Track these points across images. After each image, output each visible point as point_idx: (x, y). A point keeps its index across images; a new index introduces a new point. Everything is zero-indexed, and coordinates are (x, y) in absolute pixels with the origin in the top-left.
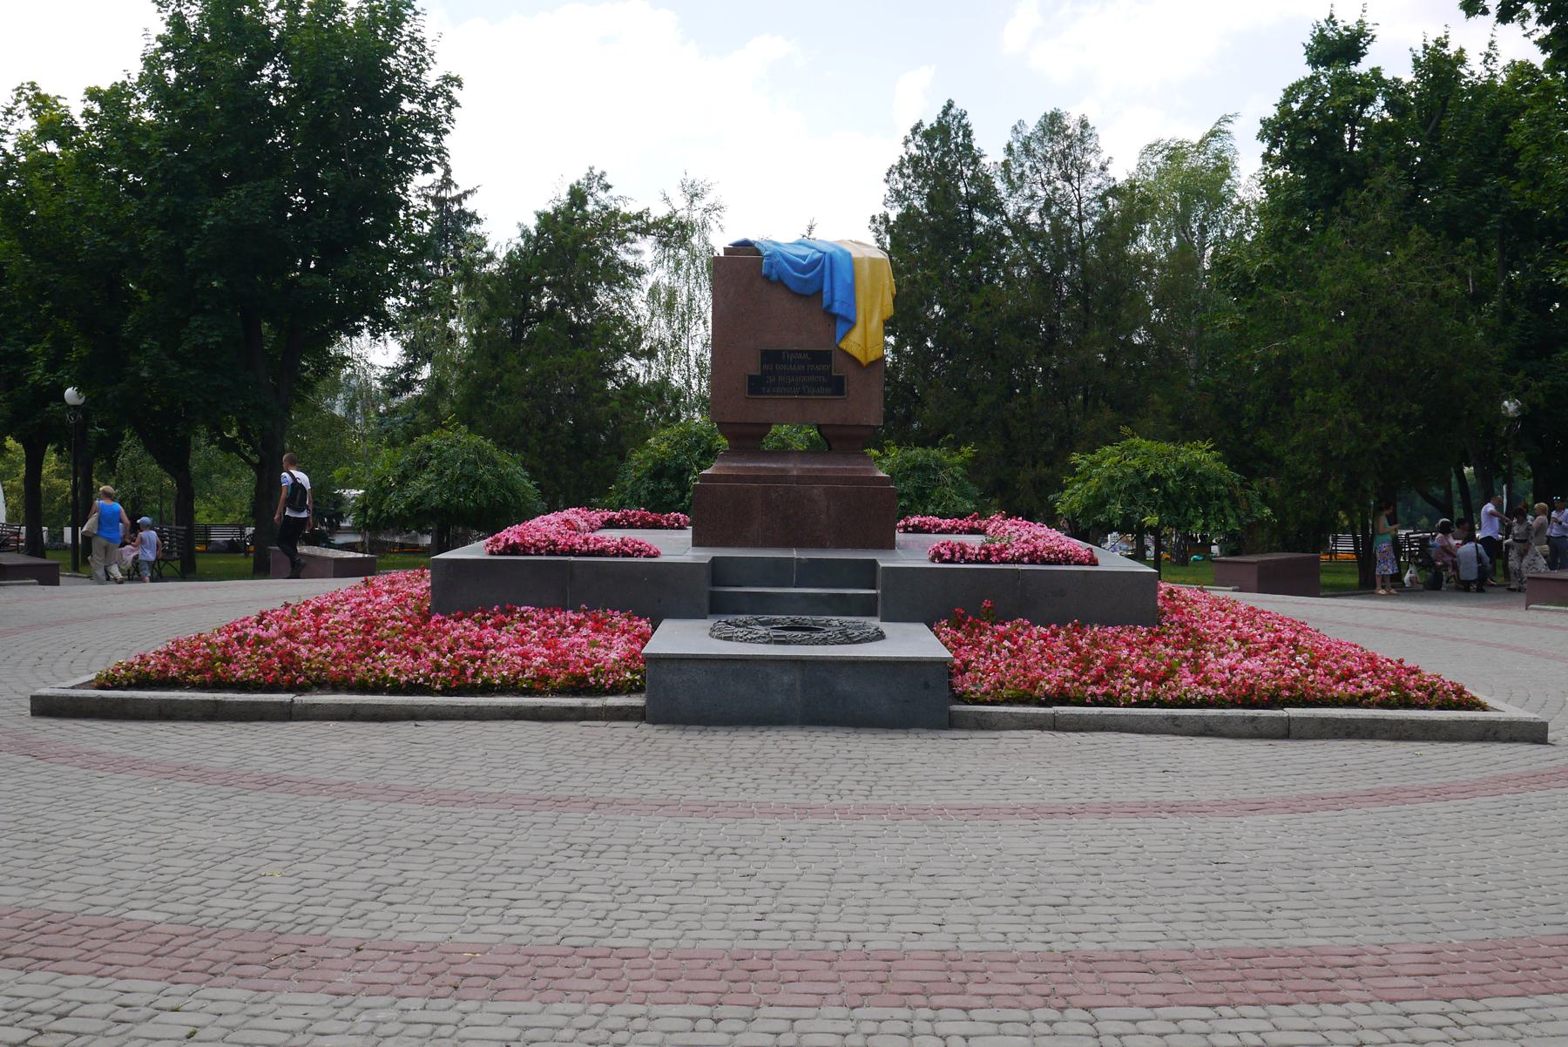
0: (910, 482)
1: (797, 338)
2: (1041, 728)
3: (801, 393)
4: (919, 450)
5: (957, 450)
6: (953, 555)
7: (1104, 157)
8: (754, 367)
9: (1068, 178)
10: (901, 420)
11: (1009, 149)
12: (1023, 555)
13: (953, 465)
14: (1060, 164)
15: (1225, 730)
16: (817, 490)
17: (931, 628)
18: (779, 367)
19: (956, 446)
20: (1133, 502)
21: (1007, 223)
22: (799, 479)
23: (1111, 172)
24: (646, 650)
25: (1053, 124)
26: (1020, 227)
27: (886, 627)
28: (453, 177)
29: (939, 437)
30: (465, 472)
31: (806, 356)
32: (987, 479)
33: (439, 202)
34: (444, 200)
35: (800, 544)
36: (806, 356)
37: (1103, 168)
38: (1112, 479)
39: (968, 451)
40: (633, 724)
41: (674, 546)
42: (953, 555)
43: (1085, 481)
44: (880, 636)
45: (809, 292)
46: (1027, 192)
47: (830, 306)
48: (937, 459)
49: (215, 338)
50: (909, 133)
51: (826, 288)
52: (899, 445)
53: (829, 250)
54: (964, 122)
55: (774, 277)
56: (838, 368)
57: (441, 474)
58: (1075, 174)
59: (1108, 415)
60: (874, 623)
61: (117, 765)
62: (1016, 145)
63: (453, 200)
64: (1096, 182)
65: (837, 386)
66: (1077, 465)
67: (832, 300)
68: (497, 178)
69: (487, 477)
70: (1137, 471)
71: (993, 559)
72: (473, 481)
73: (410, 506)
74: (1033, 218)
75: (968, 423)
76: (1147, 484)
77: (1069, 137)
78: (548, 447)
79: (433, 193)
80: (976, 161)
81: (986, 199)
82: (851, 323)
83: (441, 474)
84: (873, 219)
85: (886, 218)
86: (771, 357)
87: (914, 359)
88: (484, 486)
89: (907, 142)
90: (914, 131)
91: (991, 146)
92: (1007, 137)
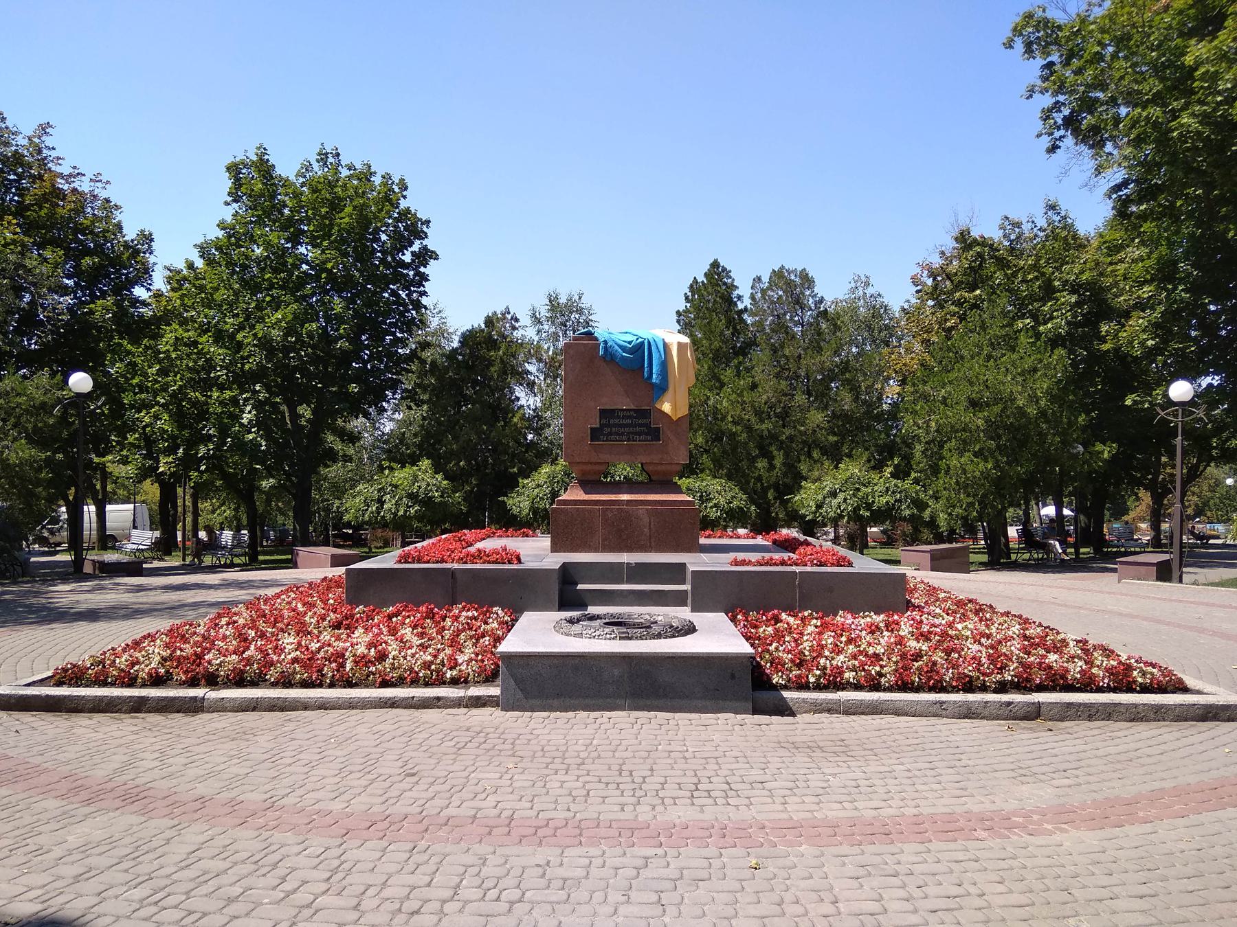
2: (829, 711)
15: (986, 712)
17: (734, 620)
22: (153, 559)
24: (504, 647)
27: (698, 618)
35: (630, 549)
40: (624, 713)
41: (536, 551)
44: (690, 629)
60: (683, 613)
61: (85, 793)
68: (455, 303)
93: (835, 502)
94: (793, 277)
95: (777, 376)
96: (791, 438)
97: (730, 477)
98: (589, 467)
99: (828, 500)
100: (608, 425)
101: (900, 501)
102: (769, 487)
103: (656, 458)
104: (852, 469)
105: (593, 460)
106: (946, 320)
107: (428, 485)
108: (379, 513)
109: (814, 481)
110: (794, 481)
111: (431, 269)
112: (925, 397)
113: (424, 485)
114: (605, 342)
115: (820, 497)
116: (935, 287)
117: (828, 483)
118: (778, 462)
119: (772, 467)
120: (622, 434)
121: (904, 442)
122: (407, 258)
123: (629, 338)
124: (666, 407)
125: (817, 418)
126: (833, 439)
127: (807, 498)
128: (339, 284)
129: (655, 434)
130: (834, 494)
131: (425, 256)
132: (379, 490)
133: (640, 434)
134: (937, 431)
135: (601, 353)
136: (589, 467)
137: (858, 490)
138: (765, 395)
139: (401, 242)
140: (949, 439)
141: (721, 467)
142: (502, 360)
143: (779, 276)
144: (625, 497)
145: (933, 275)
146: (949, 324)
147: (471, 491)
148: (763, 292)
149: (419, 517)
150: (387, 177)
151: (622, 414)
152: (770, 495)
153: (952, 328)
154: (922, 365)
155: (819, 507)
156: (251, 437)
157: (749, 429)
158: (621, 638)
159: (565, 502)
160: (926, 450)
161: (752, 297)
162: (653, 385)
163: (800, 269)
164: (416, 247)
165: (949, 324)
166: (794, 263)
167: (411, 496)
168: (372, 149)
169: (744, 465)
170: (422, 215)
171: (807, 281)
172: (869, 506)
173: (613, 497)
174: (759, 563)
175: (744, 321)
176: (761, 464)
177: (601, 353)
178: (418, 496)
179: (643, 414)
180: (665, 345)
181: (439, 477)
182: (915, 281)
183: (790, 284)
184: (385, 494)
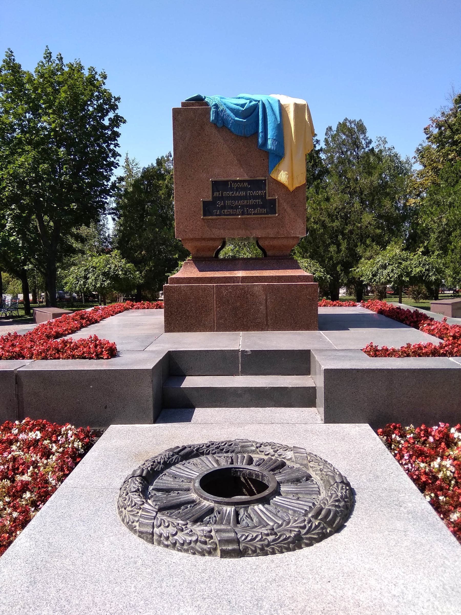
8: (207, 195)
18: (225, 194)
36: (246, 184)
93: (385, 272)
94: (353, 126)
95: (343, 192)
96: (351, 232)
97: (312, 257)
98: (204, 244)
99: (380, 271)
100: (222, 198)
101: (428, 270)
102: (338, 263)
103: (271, 233)
104: (395, 249)
105: (206, 236)
106: (448, 154)
107: (116, 266)
108: (85, 285)
109: (369, 259)
110: (355, 259)
111: (121, 129)
112: (438, 203)
113: (113, 266)
114: (216, 106)
115: (375, 269)
116: (441, 134)
117: (380, 259)
118: (343, 247)
119: (339, 251)
120: (236, 207)
121: (422, 232)
122: (106, 122)
123: (242, 101)
124: (282, 176)
125: (368, 218)
126: (378, 231)
127: (364, 269)
128: (61, 139)
129: (270, 206)
130: (384, 267)
131: (117, 121)
132: (85, 270)
133: (254, 206)
134: (446, 224)
135: (212, 118)
136: (204, 244)
137: (401, 263)
138: (336, 203)
139: (103, 113)
140: (455, 230)
141: (306, 252)
142: (167, 186)
143: (342, 127)
144: (240, 274)
145: (439, 126)
146: (450, 157)
147: (150, 270)
148: (333, 137)
149: (111, 287)
150: (91, 69)
151: (235, 186)
152: (338, 269)
153: (452, 159)
154: (433, 183)
155: (374, 275)
156: (12, 238)
157: (324, 225)
158: (225, 554)
159: (178, 280)
160: (439, 237)
161: (326, 141)
162: (268, 153)
163: (357, 120)
164: (111, 115)
165: (450, 157)
166: (354, 117)
167: (104, 274)
168: (81, 52)
169: (321, 250)
170: (115, 94)
171: (362, 128)
172: (408, 274)
173: (227, 274)
174: (406, 353)
175: (319, 157)
176: (333, 248)
177: (212, 118)
178: (109, 274)
179: (258, 184)
180: (282, 108)
181: (124, 261)
182: (426, 130)
183: (351, 131)
184: (89, 273)
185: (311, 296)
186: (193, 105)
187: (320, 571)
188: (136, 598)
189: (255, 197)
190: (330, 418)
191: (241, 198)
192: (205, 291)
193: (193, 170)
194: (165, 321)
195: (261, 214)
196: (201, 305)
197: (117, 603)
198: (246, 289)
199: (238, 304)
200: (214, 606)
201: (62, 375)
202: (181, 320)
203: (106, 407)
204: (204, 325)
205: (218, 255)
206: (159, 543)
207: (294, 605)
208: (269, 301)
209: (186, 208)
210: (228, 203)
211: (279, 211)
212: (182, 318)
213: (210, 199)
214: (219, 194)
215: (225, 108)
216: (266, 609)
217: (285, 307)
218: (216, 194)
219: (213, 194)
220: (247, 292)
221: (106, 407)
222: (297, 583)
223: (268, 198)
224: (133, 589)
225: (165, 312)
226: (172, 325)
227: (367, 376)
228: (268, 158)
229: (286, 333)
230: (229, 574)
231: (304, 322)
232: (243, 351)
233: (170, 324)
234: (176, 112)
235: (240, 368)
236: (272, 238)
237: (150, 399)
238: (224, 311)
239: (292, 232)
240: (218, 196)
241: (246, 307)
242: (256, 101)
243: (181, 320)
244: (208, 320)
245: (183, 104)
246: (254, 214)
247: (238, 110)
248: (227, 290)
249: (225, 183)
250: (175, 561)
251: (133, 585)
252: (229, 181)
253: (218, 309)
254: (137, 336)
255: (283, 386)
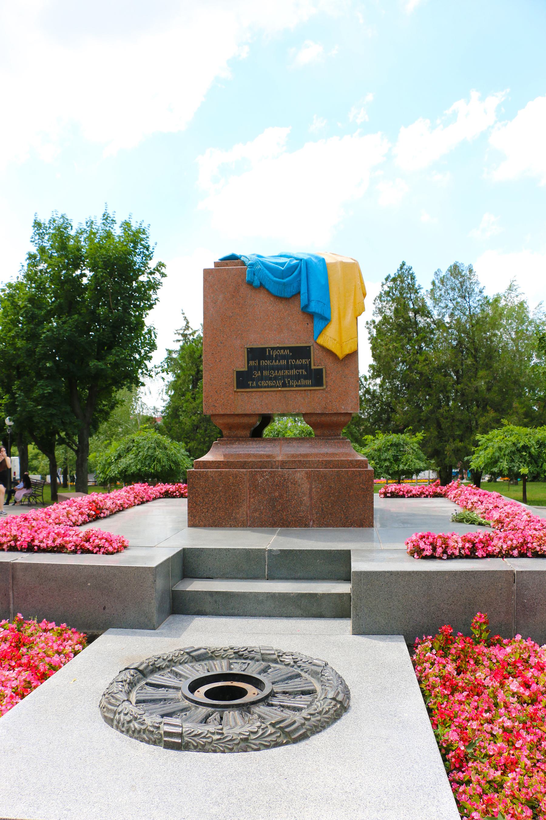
0: (390, 452)
1: (276, 330)
3: (284, 385)
4: (394, 435)
5: (414, 434)
6: (434, 549)
7: (481, 286)
9: (464, 297)
10: (384, 417)
11: (433, 283)
12: (512, 548)
13: (413, 443)
14: (459, 290)
16: (300, 474)
18: (264, 363)
19: (413, 433)
20: (512, 461)
21: (434, 322)
22: (283, 464)
23: (485, 294)
25: (455, 270)
26: (439, 324)
28: (190, 325)
29: (404, 429)
30: (149, 453)
31: (287, 352)
32: (430, 450)
33: (185, 336)
34: (186, 335)
36: (287, 352)
37: (481, 292)
38: (500, 449)
39: (420, 436)
42: (434, 549)
43: (485, 449)
45: (287, 295)
46: (443, 305)
47: (307, 306)
48: (404, 440)
49: (49, 390)
50: (384, 281)
51: (303, 290)
52: (384, 433)
53: (306, 257)
54: (411, 272)
55: (256, 283)
56: (317, 361)
57: (137, 455)
58: (467, 294)
59: (492, 414)
62: (437, 282)
63: (190, 335)
64: (478, 298)
65: (317, 378)
66: (479, 441)
67: (309, 300)
69: (160, 456)
70: (514, 444)
71: (479, 553)
72: (153, 458)
73: (120, 473)
74: (447, 319)
75: (419, 422)
76: (519, 450)
77: (463, 276)
78: (207, 439)
79: (182, 332)
80: (416, 292)
81: (423, 311)
82: (326, 320)
83: (137, 455)
84: (367, 323)
85: (374, 322)
86: (256, 354)
87: (391, 390)
88: (159, 461)
89: (383, 285)
90: (387, 279)
91: (424, 282)
92: (432, 277)
100: (260, 368)
120: (276, 378)
133: (298, 377)
151: (275, 353)
179: (302, 352)
185: (364, 485)
186: (227, 265)
187: (281, 769)
188: (91, 781)
189: (297, 367)
190: (357, 631)
191: (279, 368)
192: (236, 477)
193: (225, 336)
194: (189, 513)
195: (305, 386)
196: (232, 494)
197: (72, 784)
198: (286, 475)
199: (277, 494)
200: (163, 792)
201: (59, 570)
202: (207, 512)
203: (104, 608)
204: (235, 518)
205: (50, 460)
206: (117, 728)
207: (242, 795)
208: (314, 490)
209: (216, 379)
210: (265, 373)
211: (327, 382)
212: (208, 510)
213: (246, 369)
214: (256, 363)
215: (263, 268)
216: (213, 797)
217: (333, 499)
218: (252, 363)
219: (248, 363)
220: (288, 479)
221: (104, 608)
222: (253, 779)
223: (313, 367)
224: (90, 774)
225: (189, 502)
226: (197, 518)
227: (402, 580)
228: (313, 322)
229: (330, 530)
230: (188, 768)
231: (357, 517)
232: (270, 551)
233: (195, 516)
234: (207, 272)
235: (266, 571)
236: (319, 414)
237: (152, 601)
238: (259, 502)
239: (343, 407)
240: (254, 366)
241: (286, 497)
242: (297, 259)
243: (207, 512)
244: (241, 513)
245: (216, 264)
246: (297, 386)
247: (278, 269)
248: (263, 477)
249: (263, 350)
250: (138, 755)
251: (91, 771)
252: (267, 348)
253: (252, 500)
254: (155, 530)
255: (312, 592)
